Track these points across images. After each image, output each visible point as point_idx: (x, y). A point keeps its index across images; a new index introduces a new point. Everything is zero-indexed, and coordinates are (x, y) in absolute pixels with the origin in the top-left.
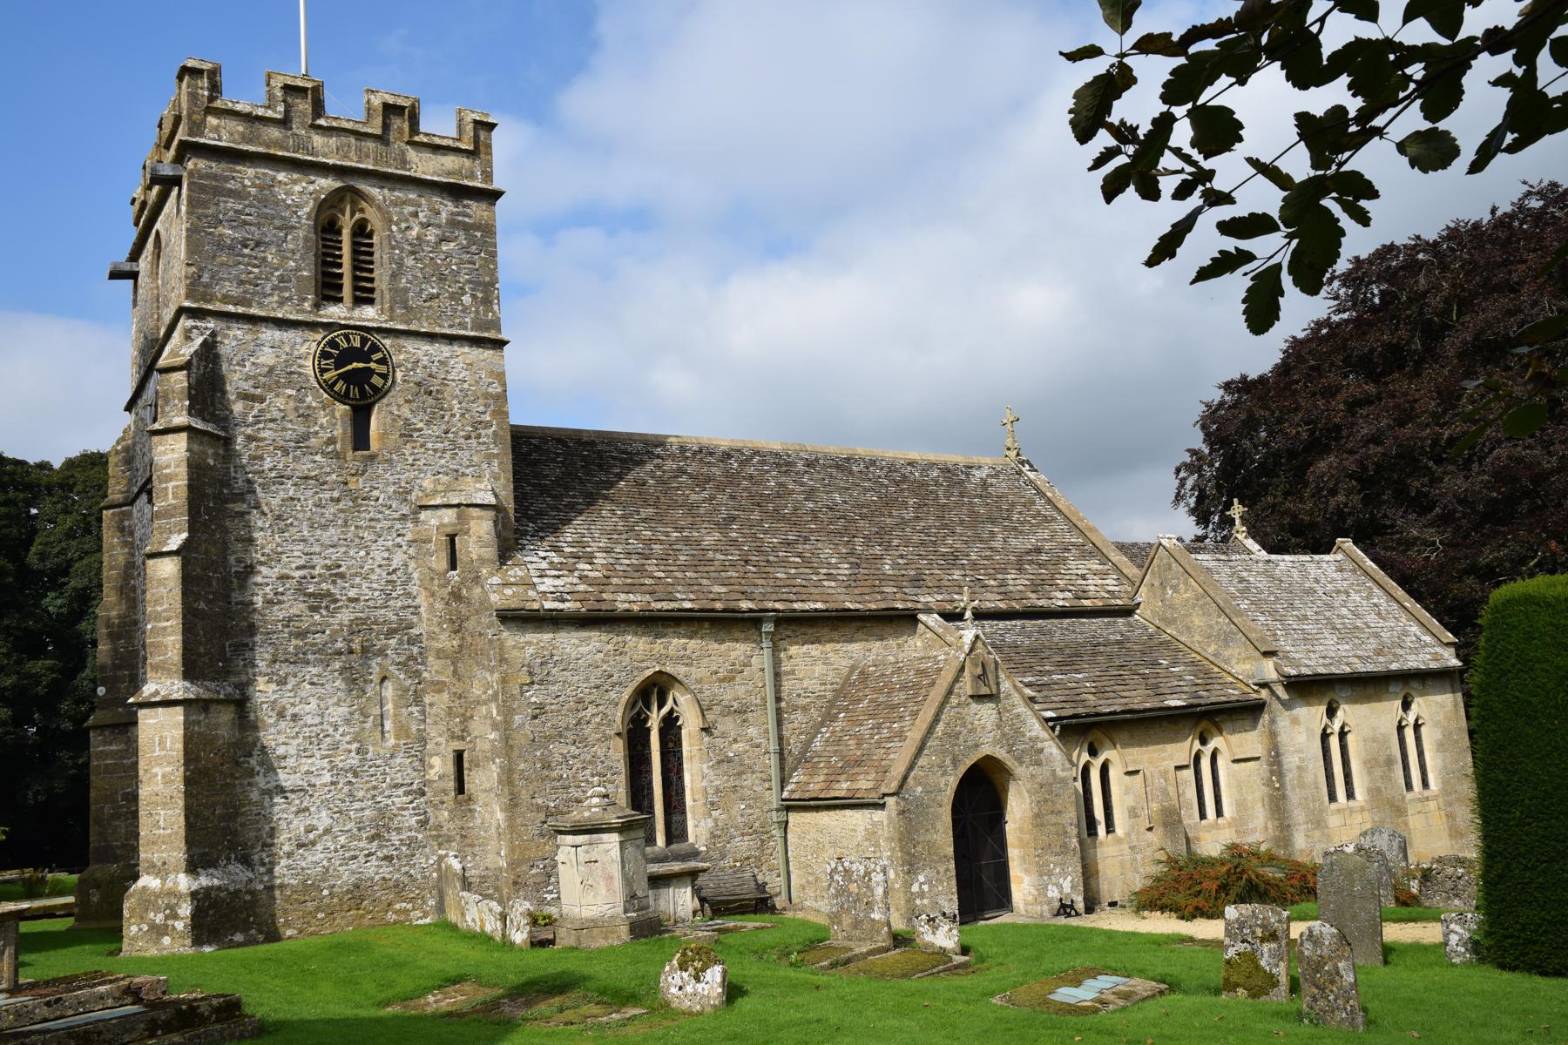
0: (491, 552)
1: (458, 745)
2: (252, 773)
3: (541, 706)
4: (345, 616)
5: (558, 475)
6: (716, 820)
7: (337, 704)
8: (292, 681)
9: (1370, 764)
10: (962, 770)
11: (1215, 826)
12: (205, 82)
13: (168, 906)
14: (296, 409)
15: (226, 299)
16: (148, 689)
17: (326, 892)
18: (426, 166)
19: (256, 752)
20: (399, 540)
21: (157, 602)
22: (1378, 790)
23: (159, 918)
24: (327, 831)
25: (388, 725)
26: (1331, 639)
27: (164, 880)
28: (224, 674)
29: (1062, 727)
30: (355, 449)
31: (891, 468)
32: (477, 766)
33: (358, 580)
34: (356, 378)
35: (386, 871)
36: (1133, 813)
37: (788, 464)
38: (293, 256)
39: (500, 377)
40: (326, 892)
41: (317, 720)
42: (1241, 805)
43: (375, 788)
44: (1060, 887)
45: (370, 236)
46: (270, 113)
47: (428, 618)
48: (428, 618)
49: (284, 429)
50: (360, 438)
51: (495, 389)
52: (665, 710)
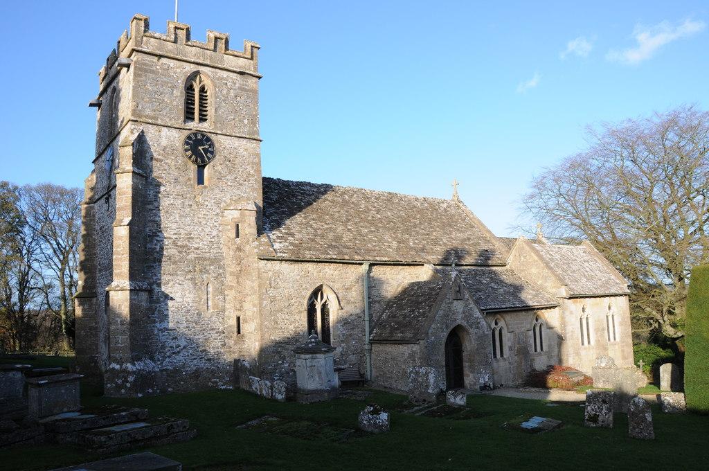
0: (254, 231)
1: (238, 313)
2: (154, 322)
3: (274, 297)
4: (192, 256)
5: (281, 201)
6: (343, 348)
7: (189, 293)
8: (171, 283)
9: (597, 330)
10: (449, 330)
11: (540, 354)
12: (142, 23)
13: (123, 377)
14: (175, 165)
15: (147, 117)
16: (114, 284)
17: (184, 373)
18: (230, 62)
19: (156, 313)
20: (215, 224)
21: (118, 246)
22: (599, 341)
23: (120, 381)
24: (184, 348)
25: (210, 303)
26: (584, 280)
27: (121, 365)
28: (144, 278)
29: (487, 313)
30: (198, 184)
31: (409, 202)
32: (246, 322)
33: (198, 240)
34: (200, 150)
35: (208, 365)
36: (511, 349)
37: (368, 198)
38: (177, 98)
39: (258, 156)
40: (184, 373)
41: (181, 300)
42: (550, 346)
43: (204, 330)
44: (484, 378)
45: (206, 92)
46: (168, 38)
47: (228, 254)
48: (228, 254)
49: (169, 174)
50: (200, 180)
51: (257, 160)
52: (323, 301)
